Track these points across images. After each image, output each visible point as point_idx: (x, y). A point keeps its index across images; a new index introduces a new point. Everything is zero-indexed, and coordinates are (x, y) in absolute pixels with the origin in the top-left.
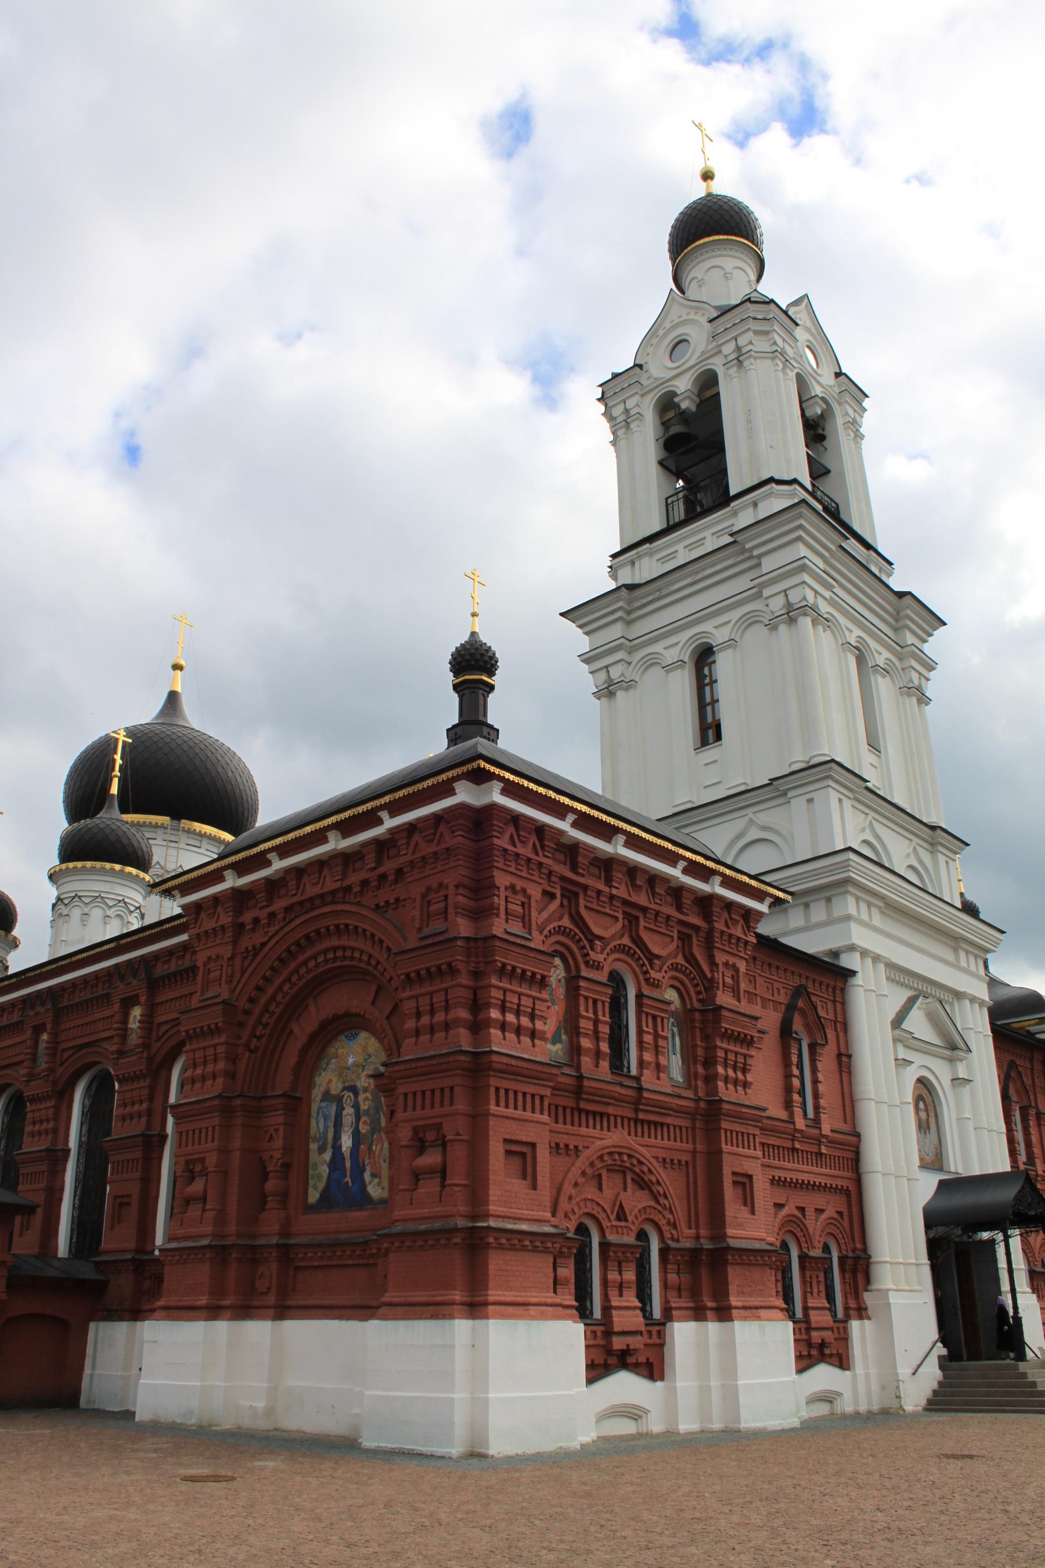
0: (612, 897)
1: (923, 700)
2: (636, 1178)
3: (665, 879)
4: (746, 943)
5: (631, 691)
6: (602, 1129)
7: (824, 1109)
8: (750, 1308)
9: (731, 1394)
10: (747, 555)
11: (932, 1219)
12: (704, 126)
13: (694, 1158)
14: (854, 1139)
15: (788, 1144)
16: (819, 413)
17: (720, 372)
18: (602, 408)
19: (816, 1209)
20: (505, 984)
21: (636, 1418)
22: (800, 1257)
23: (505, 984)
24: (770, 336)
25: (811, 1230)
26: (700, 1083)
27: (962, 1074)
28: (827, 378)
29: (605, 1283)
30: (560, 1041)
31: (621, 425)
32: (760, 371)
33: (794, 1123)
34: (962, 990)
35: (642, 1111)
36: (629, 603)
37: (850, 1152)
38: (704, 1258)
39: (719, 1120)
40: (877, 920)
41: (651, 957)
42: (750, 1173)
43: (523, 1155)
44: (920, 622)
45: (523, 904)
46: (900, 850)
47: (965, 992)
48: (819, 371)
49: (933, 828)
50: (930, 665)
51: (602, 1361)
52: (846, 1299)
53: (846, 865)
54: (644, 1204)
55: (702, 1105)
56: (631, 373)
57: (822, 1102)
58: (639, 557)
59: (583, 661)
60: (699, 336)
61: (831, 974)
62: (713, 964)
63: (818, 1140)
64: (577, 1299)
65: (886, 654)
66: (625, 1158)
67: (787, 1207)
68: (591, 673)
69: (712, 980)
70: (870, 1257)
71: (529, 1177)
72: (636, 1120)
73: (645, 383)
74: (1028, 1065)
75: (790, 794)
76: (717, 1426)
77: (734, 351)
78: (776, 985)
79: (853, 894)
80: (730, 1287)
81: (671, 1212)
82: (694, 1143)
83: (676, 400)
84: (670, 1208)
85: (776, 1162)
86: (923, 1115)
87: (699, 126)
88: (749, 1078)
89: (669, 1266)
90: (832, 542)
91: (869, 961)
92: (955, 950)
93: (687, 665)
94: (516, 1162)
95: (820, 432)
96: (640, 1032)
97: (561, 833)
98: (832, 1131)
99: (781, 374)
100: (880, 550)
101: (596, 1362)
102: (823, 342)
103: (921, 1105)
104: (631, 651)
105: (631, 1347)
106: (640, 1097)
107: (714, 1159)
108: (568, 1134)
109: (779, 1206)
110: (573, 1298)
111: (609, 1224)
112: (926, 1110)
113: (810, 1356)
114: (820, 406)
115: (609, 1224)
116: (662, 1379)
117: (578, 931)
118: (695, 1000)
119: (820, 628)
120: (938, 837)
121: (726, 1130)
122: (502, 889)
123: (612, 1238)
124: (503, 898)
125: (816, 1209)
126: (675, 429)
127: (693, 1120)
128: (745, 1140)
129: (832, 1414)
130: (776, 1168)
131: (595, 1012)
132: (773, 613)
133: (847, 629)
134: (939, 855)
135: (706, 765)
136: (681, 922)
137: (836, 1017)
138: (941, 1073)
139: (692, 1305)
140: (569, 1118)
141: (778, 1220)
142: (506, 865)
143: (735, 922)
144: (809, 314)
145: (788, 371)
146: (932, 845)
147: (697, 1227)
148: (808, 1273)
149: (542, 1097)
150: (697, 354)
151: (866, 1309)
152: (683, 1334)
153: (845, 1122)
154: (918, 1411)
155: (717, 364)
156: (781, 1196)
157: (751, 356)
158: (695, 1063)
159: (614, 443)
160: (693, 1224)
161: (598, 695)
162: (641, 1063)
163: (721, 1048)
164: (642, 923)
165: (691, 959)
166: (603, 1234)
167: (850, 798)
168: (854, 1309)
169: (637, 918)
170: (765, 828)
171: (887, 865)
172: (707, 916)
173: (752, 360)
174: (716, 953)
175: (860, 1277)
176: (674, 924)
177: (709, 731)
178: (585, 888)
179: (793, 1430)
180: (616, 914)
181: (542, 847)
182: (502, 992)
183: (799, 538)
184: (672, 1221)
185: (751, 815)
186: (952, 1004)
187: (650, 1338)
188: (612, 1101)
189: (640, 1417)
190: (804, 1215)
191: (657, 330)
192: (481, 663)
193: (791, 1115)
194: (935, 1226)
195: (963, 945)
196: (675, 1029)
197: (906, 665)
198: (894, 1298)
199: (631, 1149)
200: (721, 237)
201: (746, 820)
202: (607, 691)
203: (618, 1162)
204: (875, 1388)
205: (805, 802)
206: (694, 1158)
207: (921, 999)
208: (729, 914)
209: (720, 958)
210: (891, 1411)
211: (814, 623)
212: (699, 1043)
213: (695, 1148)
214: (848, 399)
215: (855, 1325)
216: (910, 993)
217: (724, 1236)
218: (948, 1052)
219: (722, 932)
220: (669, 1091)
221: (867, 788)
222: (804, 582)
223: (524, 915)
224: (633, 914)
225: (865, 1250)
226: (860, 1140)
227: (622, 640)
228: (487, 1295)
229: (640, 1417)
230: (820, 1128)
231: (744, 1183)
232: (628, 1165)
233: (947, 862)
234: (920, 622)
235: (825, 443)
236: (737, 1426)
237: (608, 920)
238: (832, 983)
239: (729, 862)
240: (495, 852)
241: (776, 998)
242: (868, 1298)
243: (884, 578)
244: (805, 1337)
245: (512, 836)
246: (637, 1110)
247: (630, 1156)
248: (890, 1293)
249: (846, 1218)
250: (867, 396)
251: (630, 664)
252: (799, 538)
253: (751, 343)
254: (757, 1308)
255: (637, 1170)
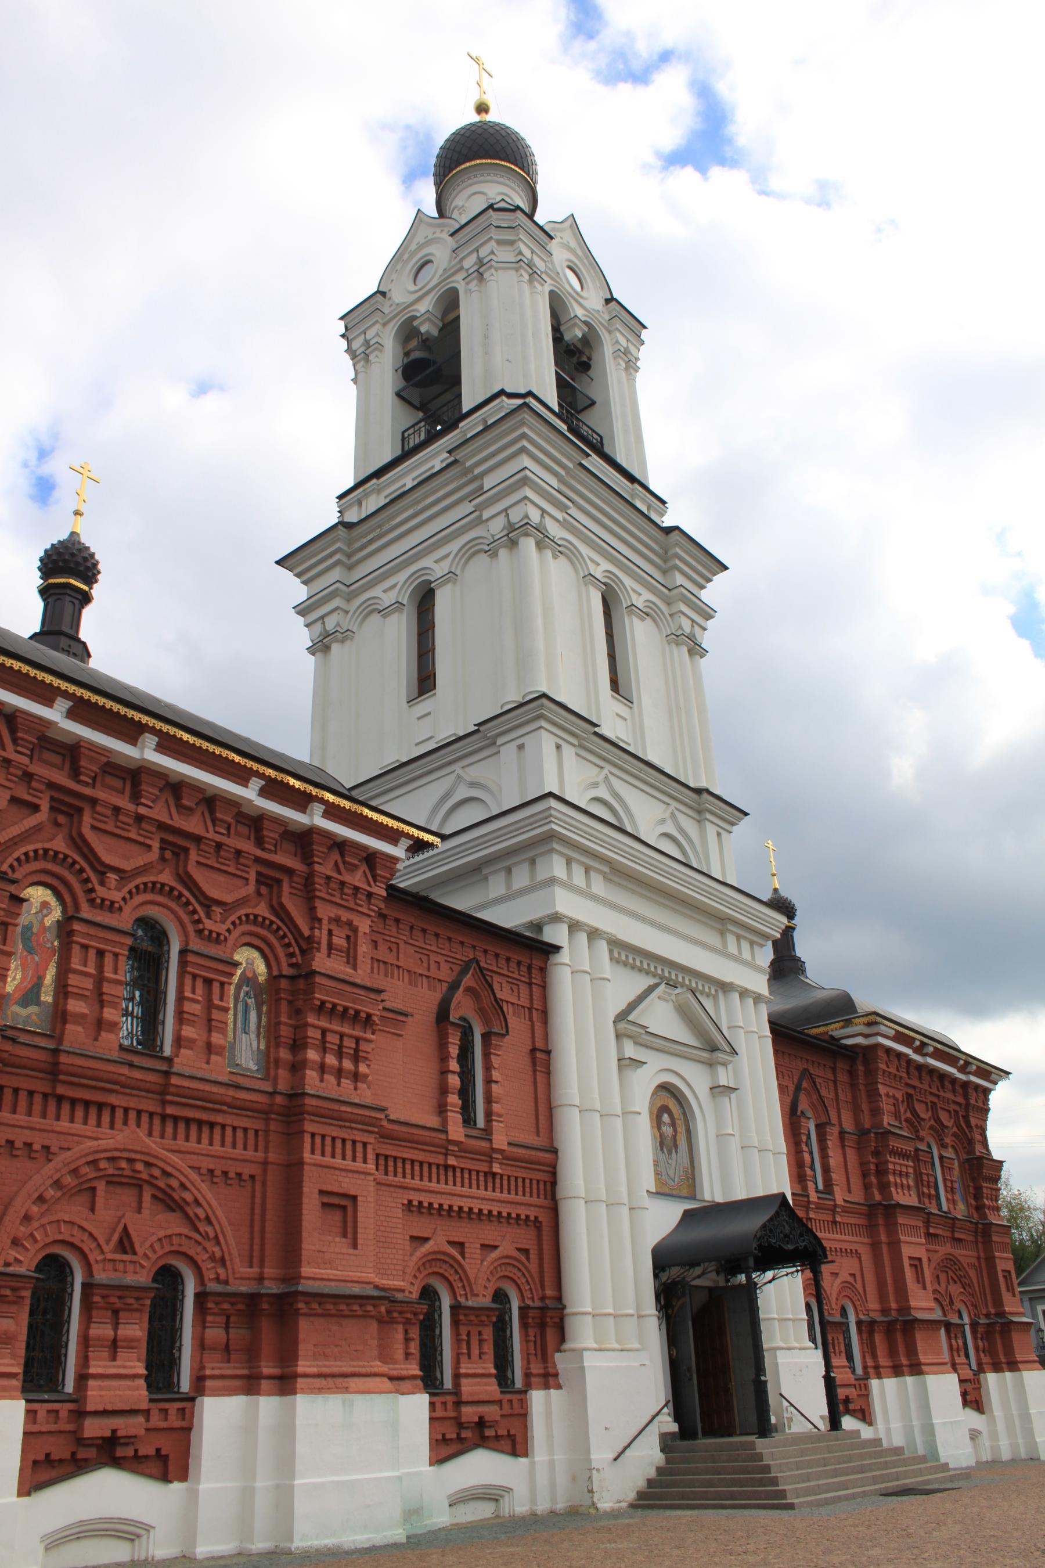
0: (139, 818)
1: (696, 650)
2: (160, 1195)
3: (234, 804)
4: (370, 895)
5: (348, 643)
6: (99, 1125)
7: (500, 1116)
8: (333, 1376)
9: (284, 1498)
10: (469, 476)
11: (663, 1259)
12: (483, 59)
13: (265, 1171)
14: (547, 1155)
15: (440, 1159)
16: (580, 336)
17: (461, 288)
18: (344, 343)
19: (482, 1245)
20: (324, 1023)
21: (132, 1538)
22: (452, 1307)
23: (324, 1023)
24: (516, 246)
25: (472, 1277)
26: (283, 1073)
27: (723, 1081)
28: (594, 301)
29: (85, 1341)
30: (38, 1003)
31: (360, 357)
32: (503, 284)
33: (447, 1132)
34: (728, 980)
35: (180, 1108)
36: (349, 544)
37: (541, 1173)
38: (265, 1306)
39: (303, 1120)
40: (598, 886)
41: (209, 903)
42: (352, 1192)
43: (344, 1208)
44: (694, 563)
45: (348, 938)
46: (648, 815)
47: (731, 984)
48: (584, 294)
49: (699, 791)
50: (708, 614)
51: (67, 1455)
52: (529, 1362)
53: (546, 816)
54: (178, 1230)
55: (279, 1100)
56: (372, 301)
57: (496, 1107)
58: (367, 495)
59: (298, 613)
60: (441, 254)
61: (532, 950)
62: (315, 920)
63: (489, 1156)
64: (496, 1367)
65: (647, 595)
66: (140, 1166)
67: (431, 1242)
68: (307, 626)
69: (310, 939)
70: (564, 1307)
71: (350, 1235)
72: (164, 1117)
73: (386, 310)
74: (831, 1076)
75: (499, 741)
76: (260, 1545)
77: (475, 264)
78: (434, 957)
79: (562, 854)
80: (301, 1347)
81: (218, 1243)
82: (266, 1151)
83: (415, 323)
84: (216, 1237)
85: (416, 1182)
86: (668, 1131)
87: (476, 60)
88: (363, 1068)
89: (209, 1318)
90: (569, 459)
91: (750, 1001)
92: (722, 933)
93: (405, 608)
94: (337, 1216)
95: (585, 359)
96: (181, 999)
97: (48, 724)
98: (509, 1144)
99: (623, 374)
100: (652, 488)
101: (448, 1436)
102: (591, 264)
103: (666, 1118)
104: (349, 598)
105: (120, 1434)
106: (167, 1085)
107: (293, 1172)
108: (32, 1129)
109: (419, 1240)
110: (417, 1367)
111: (100, 1257)
112: (673, 1124)
113: (460, 1439)
114: (580, 329)
115: (100, 1257)
116: (184, 1477)
117: (78, 858)
118: (284, 964)
119: (549, 554)
120: (703, 802)
121: (313, 1135)
122: (325, 922)
123: (101, 1276)
124: (325, 933)
125: (482, 1245)
126: (416, 355)
127: (267, 1120)
128: (353, 1148)
129: (498, 1516)
130: (414, 1189)
131: (100, 967)
132: (493, 536)
133: (633, 590)
134: (707, 823)
135: (419, 719)
136: (258, 860)
137: (531, 1003)
138: (695, 1080)
139: (245, 1372)
140: (482, 1183)
141: (414, 1258)
142: (342, 899)
143: (352, 868)
144: (574, 234)
145: (536, 284)
146: (699, 812)
147: (262, 1265)
148: (463, 1330)
149: (365, 1144)
150: (440, 272)
151: (556, 1375)
152: (219, 1416)
153: (538, 1134)
154: (619, 1510)
155: (458, 282)
156: (422, 1226)
157: (491, 267)
158: (278, 1046)
159: (355, 381)
160: (255, 1260)
161: (312, 650)
162: (179, 1041)
163: (313, 1026)
164: (193, 856)
165: (280, 911)
166: (201, 1279)
167: (574, 745)
168: (539, 1375)
169: (186, 850)
170: (473, 785)
171: (629, 830)
172: (307, 858)
173: (493, 271)
174: (318, 903)
175: (551, 1334)
176: (250, 863)
177: (425, 681)
178: (93, 802)
179: (396, 1545)
180: (148, 841)
181: (374, 877)
182: (320, 1032)
183: (523, 450)
184: (218, 1255)
185: (459, 771)
186: (715, 998)
187: (446, 1410)
188: (117, 1087)
189: (139, 1536)
190: (463, 1254)
191: (403, 254)
192: (82, 568)
193: (445, 1122)
194: (670, 1267)
195: (730, 927)
196: (251, 1002)
197: (674, 610)
198: (590, 1360)
199: (148, 1154)
200: (484, 161)
201: (453, 776)
202: (321, 647)
203: (127, 1172)
204: (562, 1480)
205: (515, 748)
206: (265, 1171)
207: (663, 986)
208: (342, 855)
209: (324, 911)
210: (582, 1510)
211: (539, 545)
212: (283, 1019)
213: (266, 1158)
214: (619, 325)
215: (537, 1398)
216: (651, 981)
217: (297, 1278)
218: (705, 1055)
219: (329, 878)
220: (224, 1079)
221: (596, 734)
222: (526, 498)
223: (349, 948)
224: (176, 846)
225: (559, 1298)
226: (557, 1158)
227: (338, 585)
228: (260, 1367)
229: (139, 1536)
230: (491, 1140)
231: (342, 1207)
232: (144, 1176)
233: (719, 834)
234: (694, 563)
235: (591, 373)
236: (288, 1545)
237: (136, 848)
238: (526, 960)
239: (434, 828)
240: (317, 879)
241: (434, 972)
242: (561, 1361)
243: (654, 516)
244: (451, 1414)
245: (336, 863)
246: (164, 1103)
247: (148, 1164)
248: (586, 1354)
249: (533, 1256)
250: (645, 327)
251: (347, 612)
252: (523, 450)
253: (492, 253)
254: (345, 1375)
255: (161, 1184)
